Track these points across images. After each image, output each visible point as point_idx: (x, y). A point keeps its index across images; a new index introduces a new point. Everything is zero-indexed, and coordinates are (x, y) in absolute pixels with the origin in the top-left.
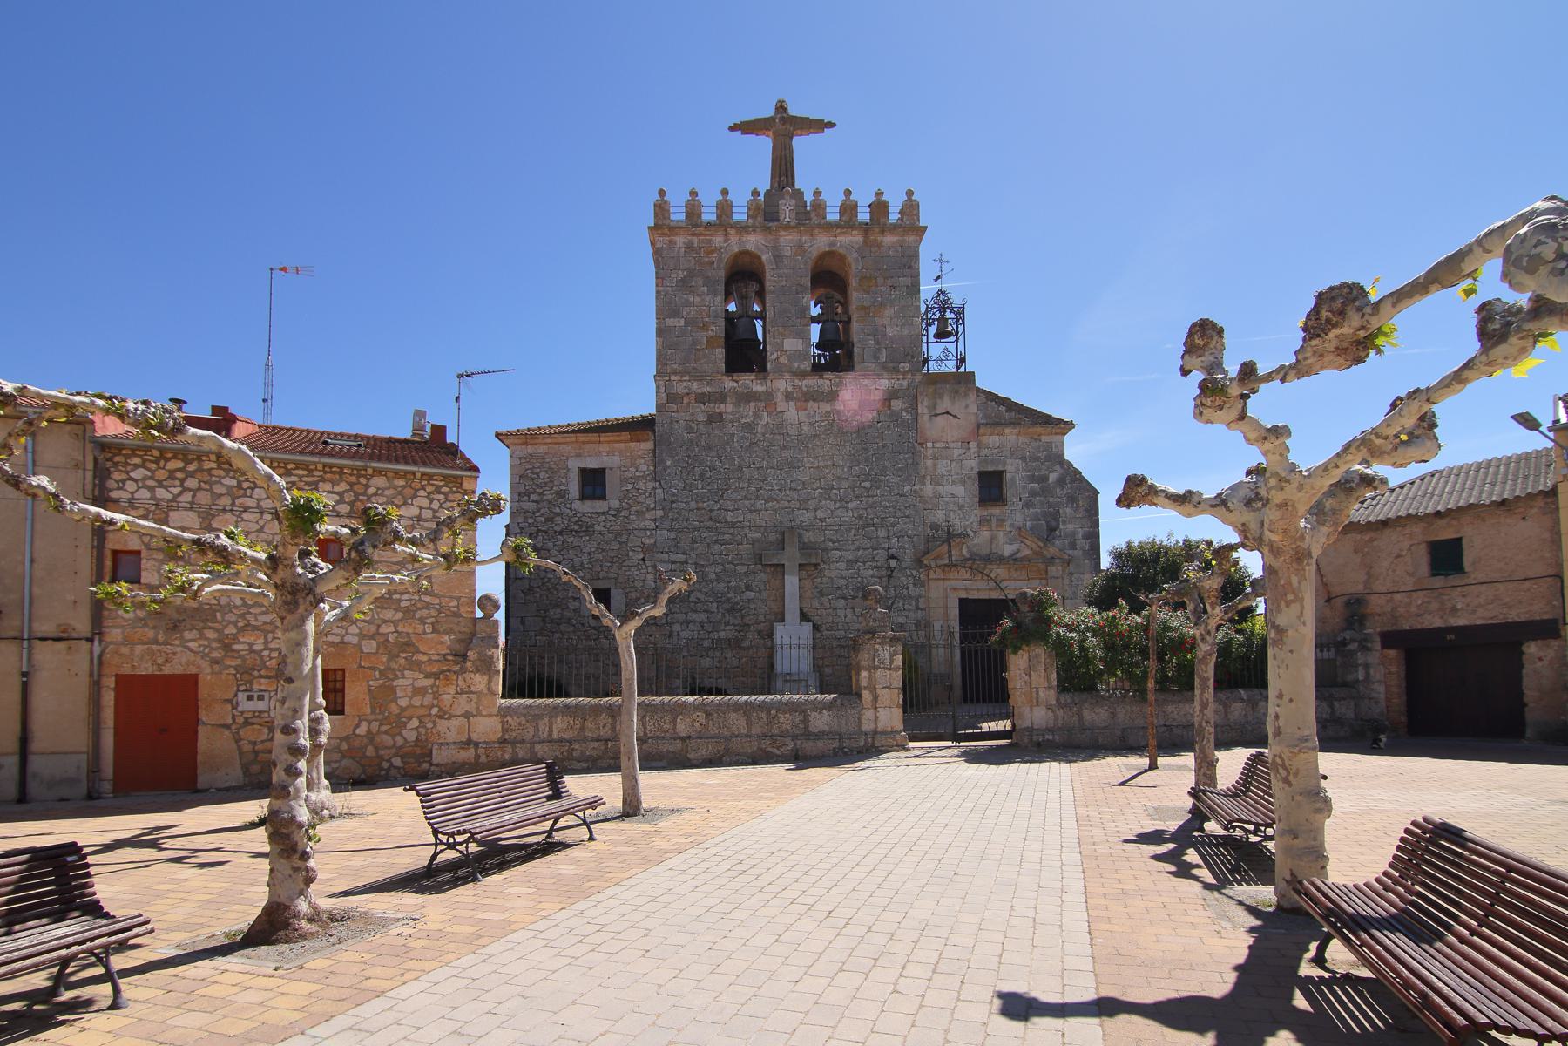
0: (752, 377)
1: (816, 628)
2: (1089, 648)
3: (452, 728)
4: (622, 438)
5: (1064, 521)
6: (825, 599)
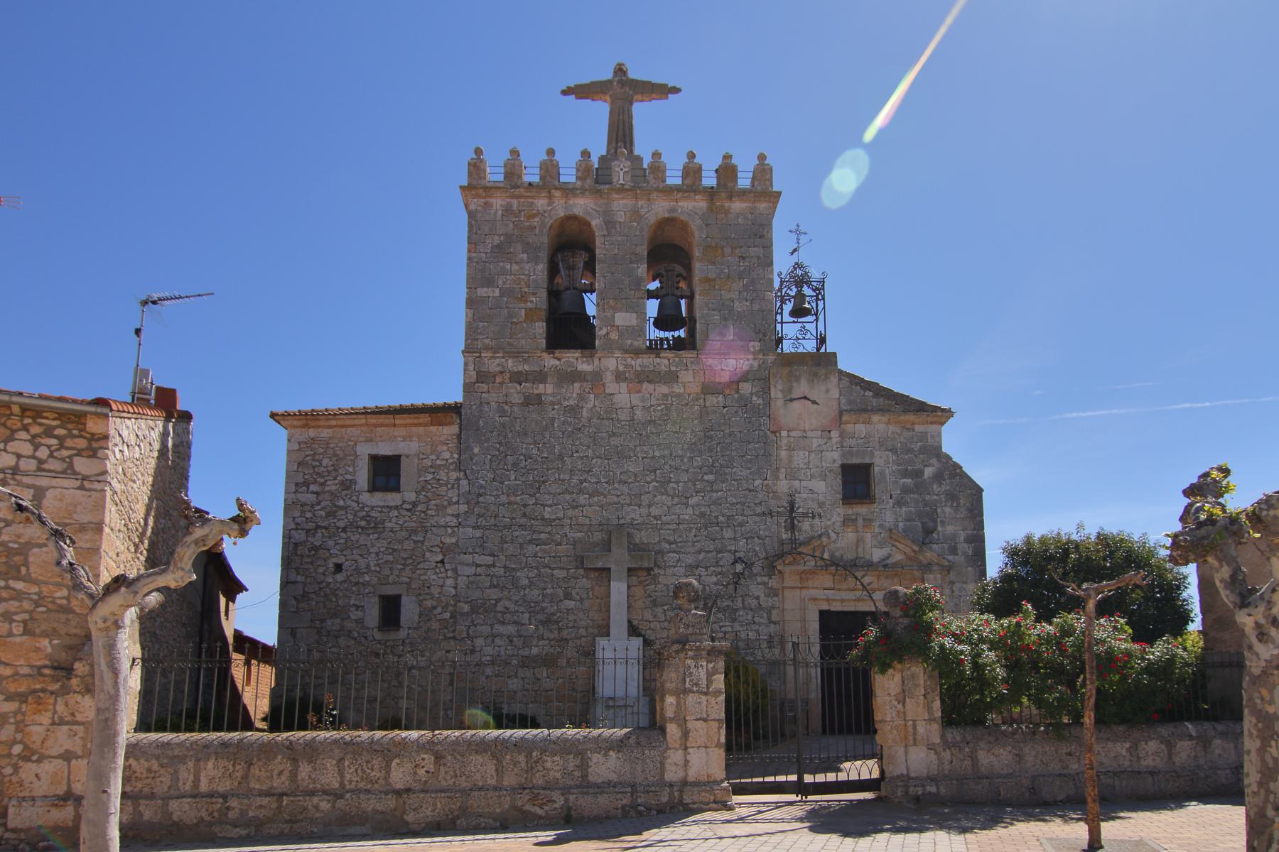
0: (577, 355)
1: (647, 643)
2: (986, 665)
3: (43, 776)
4: (421, 421)
5: (942, 522)
6: (659, 610)
